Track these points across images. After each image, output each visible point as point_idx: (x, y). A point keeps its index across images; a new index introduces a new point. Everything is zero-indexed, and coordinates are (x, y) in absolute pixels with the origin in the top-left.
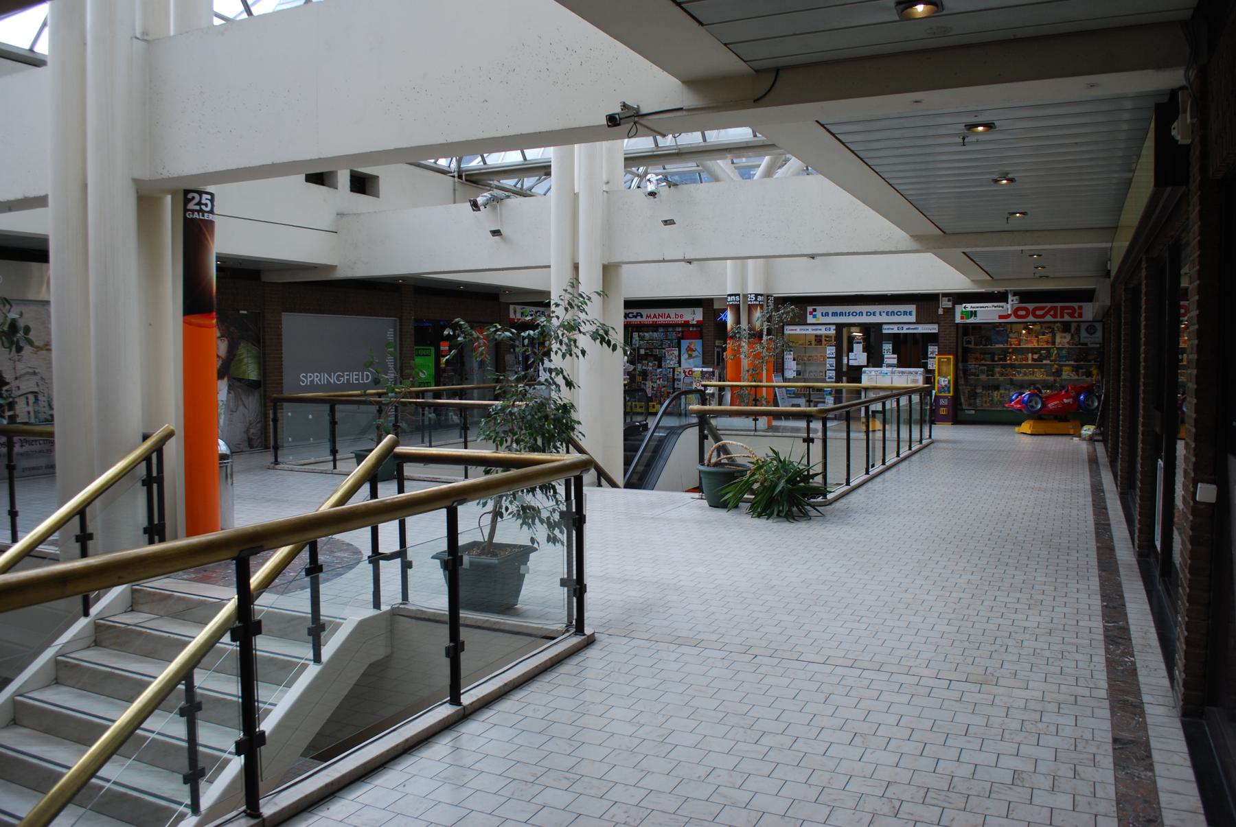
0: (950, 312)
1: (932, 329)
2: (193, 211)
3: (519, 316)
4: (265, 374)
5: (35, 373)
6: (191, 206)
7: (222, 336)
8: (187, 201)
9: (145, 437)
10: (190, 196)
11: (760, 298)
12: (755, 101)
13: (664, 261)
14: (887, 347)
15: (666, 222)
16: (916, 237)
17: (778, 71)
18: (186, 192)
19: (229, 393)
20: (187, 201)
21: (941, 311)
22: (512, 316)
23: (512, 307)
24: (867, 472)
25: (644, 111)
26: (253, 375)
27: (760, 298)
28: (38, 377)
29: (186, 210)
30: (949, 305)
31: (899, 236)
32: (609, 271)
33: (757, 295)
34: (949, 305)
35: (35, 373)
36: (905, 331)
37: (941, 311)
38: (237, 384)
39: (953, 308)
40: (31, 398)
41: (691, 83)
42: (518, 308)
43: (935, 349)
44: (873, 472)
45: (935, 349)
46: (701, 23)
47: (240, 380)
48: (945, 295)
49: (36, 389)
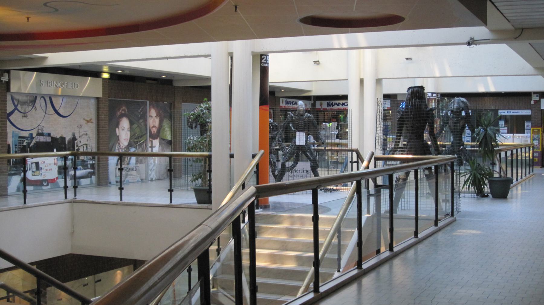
0: (538, 103)
1: (528, 112)
2: (264, 63)
3: (284, 105)
4: (174, 136)
5: (86, 134)
6: (263, 61)
7: (157, 116)
8: (262, 59)
9: (254, 156)
10: (263, 57)
11: (434, 95)
12: (515, 38)
13: (408, 78)
14: (501, 123)
15: (407, 59)
16: (537, 68)
17: (523, 29)
18: (261, 55)
19: (159, 147)
20: (262, 59)
21: (532, 102)
22: (281, 105)
23: (281, 99)
24: (436, 224)
25: (475, 39)
26: (169, 137)
27: (434, 95)
28: (88, 136)
29: (261, 63)
30: (537, 99)
31: (528, 67)
32: (379, 81)
33: (432, 93)
34: (537, 99)
35: (86, 134)
36: (512, 114)
37: (532, 102)
38: (163, 142)
39: (540, 101)
40: (85, 146)
41: (492, 31)
42: (285, 100)
43: (530, 124)
44: (440, 224)
45: (530, 124)
46: (509, 21)
47: (164, 140)
48: (535, 93)
49: (86, 143)
